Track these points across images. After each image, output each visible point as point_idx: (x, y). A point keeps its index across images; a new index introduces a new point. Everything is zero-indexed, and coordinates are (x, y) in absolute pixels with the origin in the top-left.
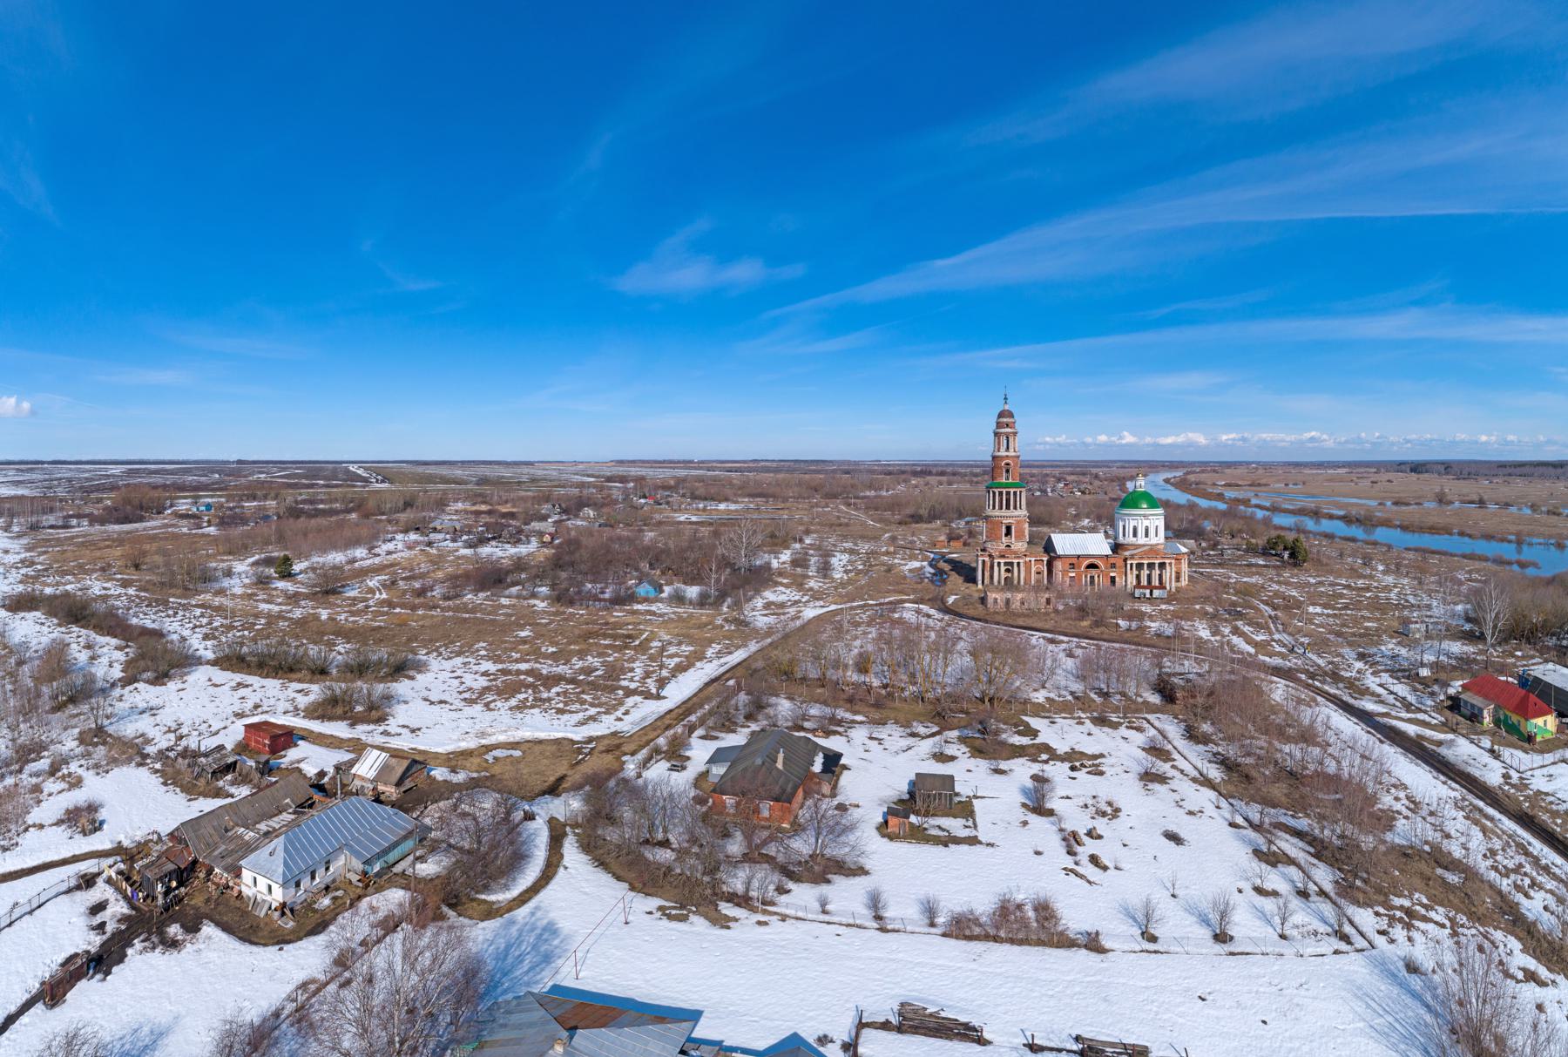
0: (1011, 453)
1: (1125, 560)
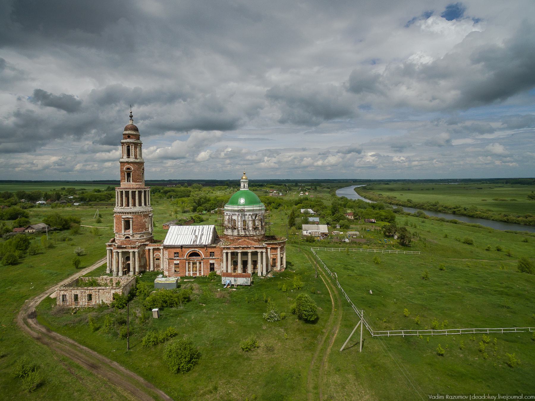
0: (132, 159)
1: (222, 251)
